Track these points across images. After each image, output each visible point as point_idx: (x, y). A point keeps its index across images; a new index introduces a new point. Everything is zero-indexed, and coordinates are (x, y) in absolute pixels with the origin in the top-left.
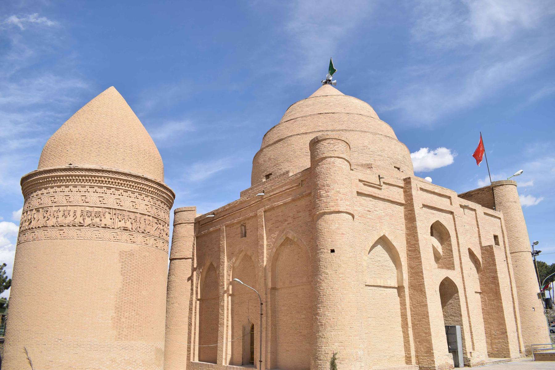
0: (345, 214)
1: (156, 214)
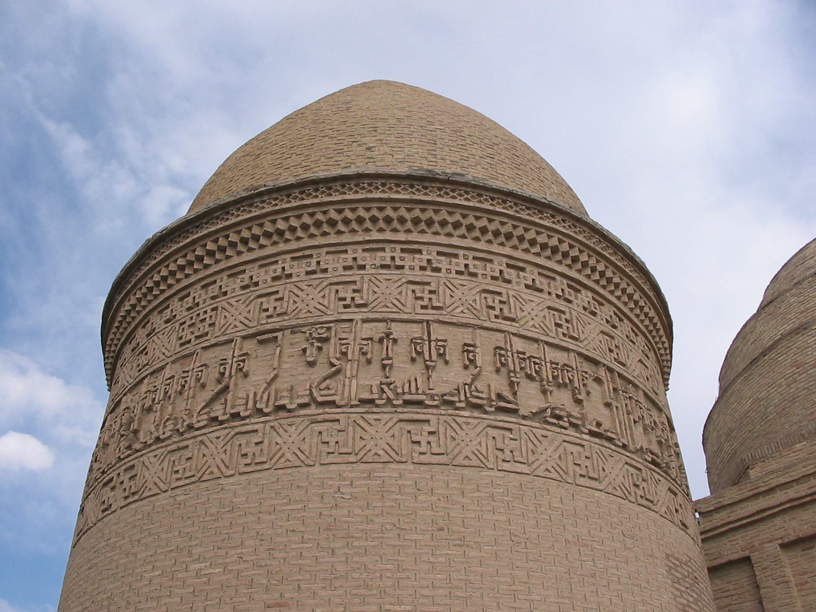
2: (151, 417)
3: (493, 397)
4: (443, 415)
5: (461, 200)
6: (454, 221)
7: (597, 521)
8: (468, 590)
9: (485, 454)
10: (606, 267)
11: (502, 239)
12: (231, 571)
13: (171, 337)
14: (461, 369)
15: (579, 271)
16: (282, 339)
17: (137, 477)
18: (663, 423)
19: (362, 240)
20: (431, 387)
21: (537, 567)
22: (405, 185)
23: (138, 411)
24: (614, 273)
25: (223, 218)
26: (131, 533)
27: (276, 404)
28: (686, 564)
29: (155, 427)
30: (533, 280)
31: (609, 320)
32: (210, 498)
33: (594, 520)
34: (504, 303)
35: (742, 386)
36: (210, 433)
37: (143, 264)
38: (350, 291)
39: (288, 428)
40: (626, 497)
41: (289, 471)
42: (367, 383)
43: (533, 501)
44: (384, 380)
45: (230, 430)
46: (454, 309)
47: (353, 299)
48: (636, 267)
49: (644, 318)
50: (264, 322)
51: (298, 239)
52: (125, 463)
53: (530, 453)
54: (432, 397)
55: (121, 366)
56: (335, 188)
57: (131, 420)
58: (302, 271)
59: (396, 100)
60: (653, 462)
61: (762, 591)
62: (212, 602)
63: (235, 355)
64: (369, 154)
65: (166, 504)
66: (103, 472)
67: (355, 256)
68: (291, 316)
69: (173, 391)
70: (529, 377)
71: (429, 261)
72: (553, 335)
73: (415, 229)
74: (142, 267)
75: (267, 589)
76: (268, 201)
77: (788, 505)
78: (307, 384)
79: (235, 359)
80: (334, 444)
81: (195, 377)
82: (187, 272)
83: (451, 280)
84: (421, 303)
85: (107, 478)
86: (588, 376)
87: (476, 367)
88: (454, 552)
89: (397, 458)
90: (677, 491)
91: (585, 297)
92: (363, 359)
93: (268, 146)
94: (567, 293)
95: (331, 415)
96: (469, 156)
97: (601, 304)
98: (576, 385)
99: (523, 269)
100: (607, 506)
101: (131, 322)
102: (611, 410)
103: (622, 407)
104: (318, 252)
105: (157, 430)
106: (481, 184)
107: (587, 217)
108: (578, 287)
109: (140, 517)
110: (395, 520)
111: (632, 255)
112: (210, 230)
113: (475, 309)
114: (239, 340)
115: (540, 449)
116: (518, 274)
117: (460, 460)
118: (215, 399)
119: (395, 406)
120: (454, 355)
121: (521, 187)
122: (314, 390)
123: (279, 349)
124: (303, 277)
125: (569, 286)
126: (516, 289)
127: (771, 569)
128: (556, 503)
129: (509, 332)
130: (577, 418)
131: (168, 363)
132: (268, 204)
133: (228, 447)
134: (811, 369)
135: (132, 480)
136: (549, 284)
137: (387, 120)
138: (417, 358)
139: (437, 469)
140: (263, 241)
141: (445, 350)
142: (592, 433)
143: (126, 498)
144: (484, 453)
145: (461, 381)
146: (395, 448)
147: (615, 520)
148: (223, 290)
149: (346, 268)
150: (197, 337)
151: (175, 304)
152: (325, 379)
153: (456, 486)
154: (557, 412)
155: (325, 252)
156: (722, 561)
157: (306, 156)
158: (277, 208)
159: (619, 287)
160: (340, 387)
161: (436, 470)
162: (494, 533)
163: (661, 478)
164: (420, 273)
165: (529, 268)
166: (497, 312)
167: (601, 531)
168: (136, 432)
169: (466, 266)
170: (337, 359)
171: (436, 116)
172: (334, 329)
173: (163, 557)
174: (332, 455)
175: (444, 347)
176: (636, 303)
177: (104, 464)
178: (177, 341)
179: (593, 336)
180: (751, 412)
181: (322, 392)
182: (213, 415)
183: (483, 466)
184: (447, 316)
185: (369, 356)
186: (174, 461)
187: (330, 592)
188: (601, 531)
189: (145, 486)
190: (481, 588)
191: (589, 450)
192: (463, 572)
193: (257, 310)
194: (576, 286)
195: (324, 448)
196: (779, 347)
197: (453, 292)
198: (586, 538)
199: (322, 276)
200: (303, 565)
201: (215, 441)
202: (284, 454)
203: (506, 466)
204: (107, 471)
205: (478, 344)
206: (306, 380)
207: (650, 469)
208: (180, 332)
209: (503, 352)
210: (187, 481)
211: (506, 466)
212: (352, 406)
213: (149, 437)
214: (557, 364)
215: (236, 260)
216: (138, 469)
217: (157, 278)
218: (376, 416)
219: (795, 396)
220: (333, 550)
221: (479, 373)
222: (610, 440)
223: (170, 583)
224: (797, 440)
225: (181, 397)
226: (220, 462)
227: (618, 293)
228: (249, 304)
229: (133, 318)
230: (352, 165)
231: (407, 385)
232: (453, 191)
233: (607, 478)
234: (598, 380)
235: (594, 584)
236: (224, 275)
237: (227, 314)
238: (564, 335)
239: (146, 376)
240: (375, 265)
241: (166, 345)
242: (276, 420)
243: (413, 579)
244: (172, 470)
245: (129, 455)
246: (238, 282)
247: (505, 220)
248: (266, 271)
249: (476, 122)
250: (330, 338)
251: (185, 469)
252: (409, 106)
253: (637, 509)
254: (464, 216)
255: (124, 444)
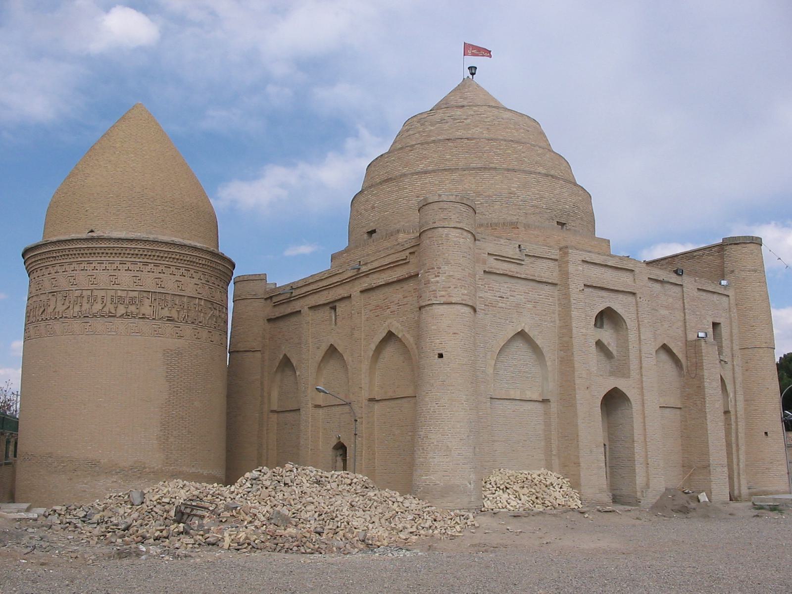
0: (459, 307)
1: (210, 297)
84: (135, 284)
117: (96, 333)
120: (99, 300)
156: (295, 311)
247: (118, 249)
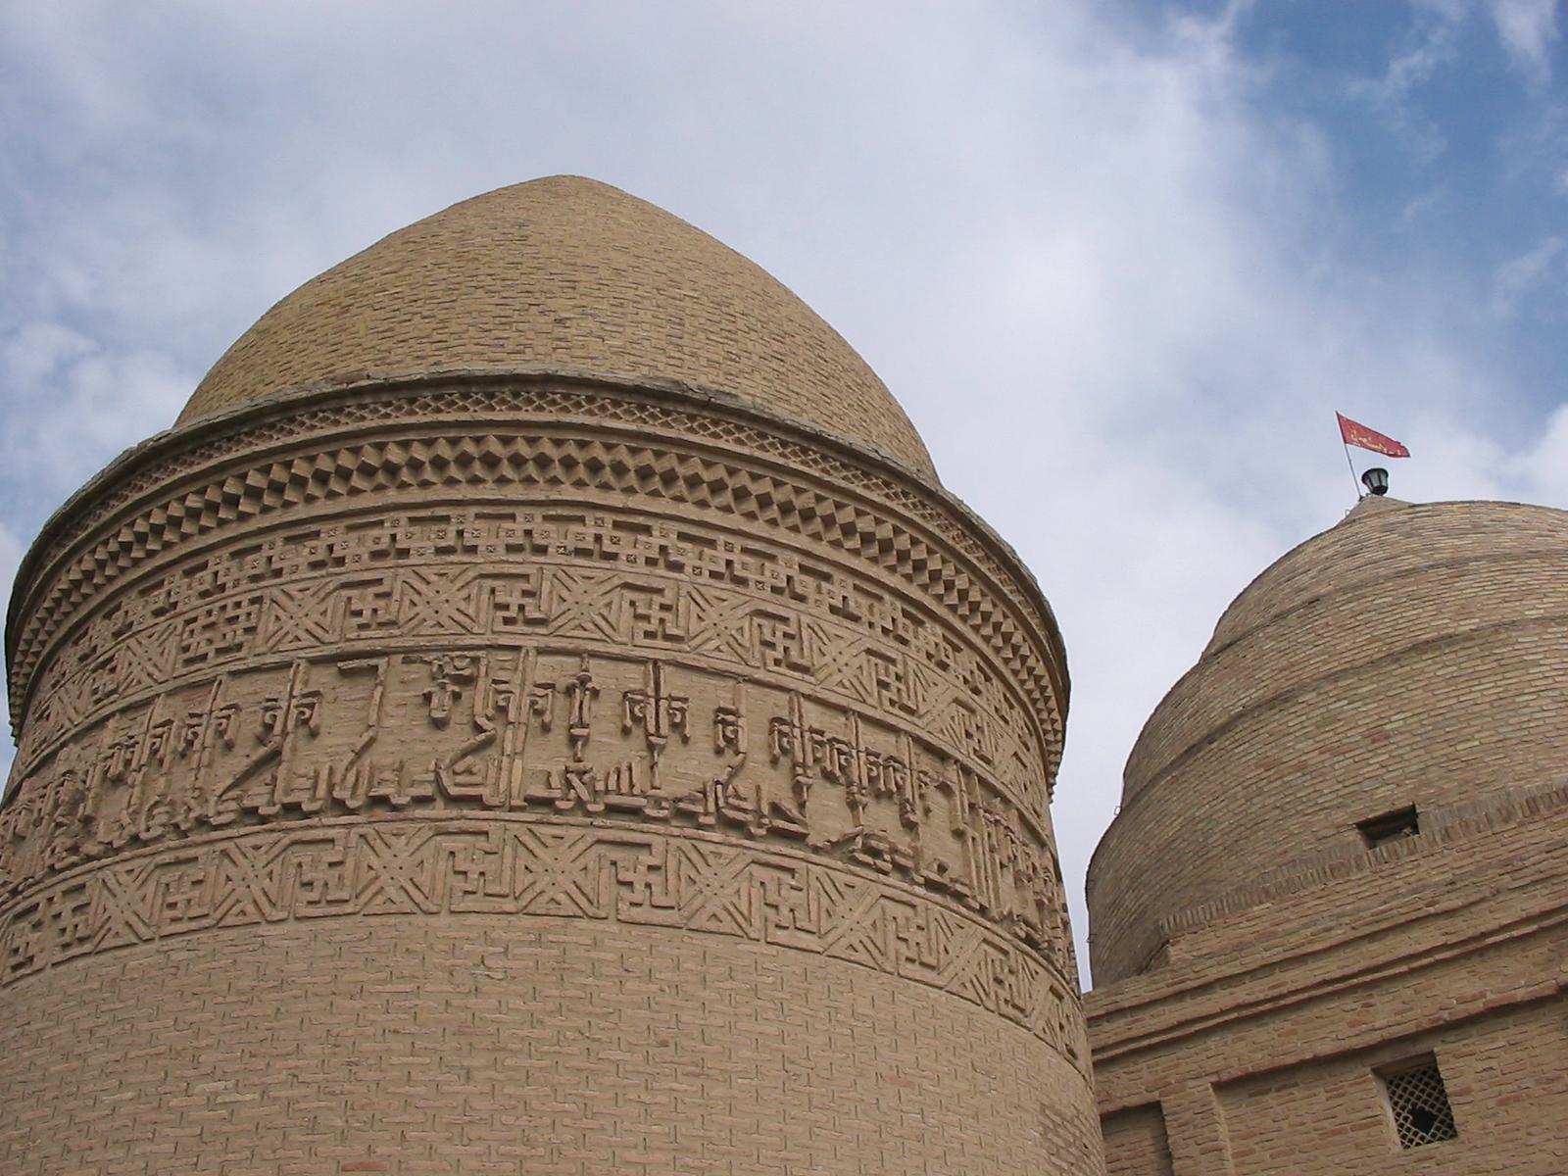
2: (121, 795)
3: (766, 809)
4: (674, 836)
5: (727, 441)
6: (712, 479)
7: (932, 1041)
8: (707, 1156)
9: (746, 913)
10: (971, 582)
11: (795, 519)
12: (275, 1099)
13: (167, 644)
14: (711, 755)
15: (924, 588)
16: (386, 671)
17: (91, 910)
18: (1046, 868)
19: (543, 498)
20: (657, 783)
21: (826, 1119)
22: (629, 403)
23: (94, 780)
24: (983, 595)
25: (282, 429)
26: (76, 1015)
27: (372, 794)
28: (1071, 1122)
29: (129, 815)
30: (844, 598)
31: (970, 679)
32: (238, 960)
33: (927, 1041)
34: (791, 637)
35: (1167, 792)
36: (241, 836)
37: (115, 496)
38: (517, 594)
39: (393, 841)
40: (982, 1000)
41: (392, 920)
42: (541, 767)
43: (826, 1002)
44: (573, 765)
45: (281, 835)
46: (704, 643)
47: (522, 608)
48: (1021, 585)
49: (1026, 677)
50: (353, 635)
51: (425, 484)
52: (64, 880)
53: (824, 915)
54: (658, 803)
55: (54, 686)
56: (500, 396)
57: (78, 796)
58: (429, 546)
59: (610, 230)
60: (1029, 940)
61: (1176, 1164)
62: (238, 1156)
63: (295, 693)
64: (559, 331)
65: (150, 966)
66: (15, 892)
67: (528, 527)
68: (405, 630)
69: (169, 750)
70: (828, 776)
71: (663, 549)
72: (874, 703)
73: (642, 487)
74: (112, 502)
75: (343, 1137)
76: (372, 406)
77: (1235, 1015)
78: (430, 762)
79: (294, 702)
80: (476, 876)
81: (213, 727)
82: (204, 522)
83: (701, 589)
84: (644, 626)
85: (25, 904)
86: (928, 780)
87: (737, 753)
88: (685, 1087)
89: (591, 911)
90: (1064, 993)
91: (932, 633)
92: (535, 722)
93: (366, 292)
94: (900, 626)
95: (473, 822)
96: (740, 353)
97: (956, 649)
98: (909, 795)
99: (827, 578)
100: (948, 1016)
101: (80, 604)
102: (964, 843)
103: (983, 839)
104: (461, 512)
105: (134, 821)
106: (766, 416)
107: (939, 488)
108: (920, 616)
109: (96, 985)
110: (582, 1023)
111: (1017, 562)
112: (257, 449)
113: (740, 645)
114: (303, 665)
115: (842, 908)
116: (819, 587)
117: (701, 921)
118: (253, 774)
119: (589, 814)
120: (699, 728)
121: (828, 420)
122: (443, 775)
123: (380, 689)
124: (430, 557)
125: (906, 614)
126: (814, 613)
127: (1195, 1127)
128: (863, 1008)
129: (797, 693)
130: (905, 856)
131: (158, 695)
132: (371, 411)
133: (276, 867)
134: (1290, 773)
135: (78, 913)
136: (871, 607)
137: (595, 270)
138: (633, 729)
139: (660, 934)
140: (357, 481)
141: (683, 717)
142: (930, 885)
143: (66, 946)
144: (744, 909)
145: (708, 776)
146: (587, 890)
147: (961, 1040)
148: (275, 566)
149: (510, 549)
150: (219, 651)
151: (176, 581)
152: (465, 754)
153: (693, 967)
154: (874, 843)
155: (473, 515)
157: (442, 321)
158: (390, 422)
159: (989, 620)
160: (492, 772)
161: (658, 936)
162: (755, 1055)
163: (1039, 969)
164: (646, 570)
165: (837, 576)
166: (779, 654)
167: (936, 1060)
168: (87, 821)
169: (729, 563)
170: (488, 719)
171: (685, 271)
172: (484, 662)
173: (141, 1066)
174: (472, 896)
175: (682, 711)
176: (1016, 649)
177: (17, 875)
178: (178, 654)
179: (940, 706)
180: (1180, 840)
181: (459, 779)
182: (247, 803)
183: (740, 933)
184: (691, 655)
185: (547, 718)
186: (167, 885)
187: (460, 1147)
188: (936, 1060)
189: (106, 927)
190: (729, 1153)
191: (924, 915)
192: (698, 1124)
193: (341, 611)
194: (917, 614)
195: (459, 883)
196: (1238, 730)
197: (704, 610)
198: (912, 1071)
199: (466, 558)
200: (411, 1096)
201: (250, 853)
202: (382, 888)
203: (781, 936)
204: (22, 891)
205: (743, 711)
206: (427, 753)
207: (1024, 952)
208: (185, 636)
209: (785, 729)
210: (194, 925)
211: (781, 936)
212: (512, 809)
213: (118, 834)
214: (877, 756)
215: (301, 512)
216: (94, 892)
217: (141, 526)
218: (556, 831)
219: (1259, 819)
220: (468, 1073)
221: (742, 765)
222: (959, 897)
223: (154, 1116)
224: (1255, 898)
225: (184, 762)
226: (261, 894)
227: (987, 631)
228: (323, 599)
229: (86, 597)
230: (527, 350)
231: (613, 778)
232: (716, 423)
233: (952, 967)
234: (945, 789)
235: (920, 1153)
236: (278, 538)
237: (281, 613)
238: (892, 703)
239: (113, 714)
240: (565, 547)
241: (156, 658)
242: (370, 823)
243: (611, 1130)
244: (163, 901)
245: (73, 865)
246: (303, 554)
247: (803, 485)
248: (359, 539)
249: (755, 289)
250: (477, 677)
251: (189, 901)
252: (636, 246)
253: (999, 1023)
254: (732, 472)
255: (62, 841)
